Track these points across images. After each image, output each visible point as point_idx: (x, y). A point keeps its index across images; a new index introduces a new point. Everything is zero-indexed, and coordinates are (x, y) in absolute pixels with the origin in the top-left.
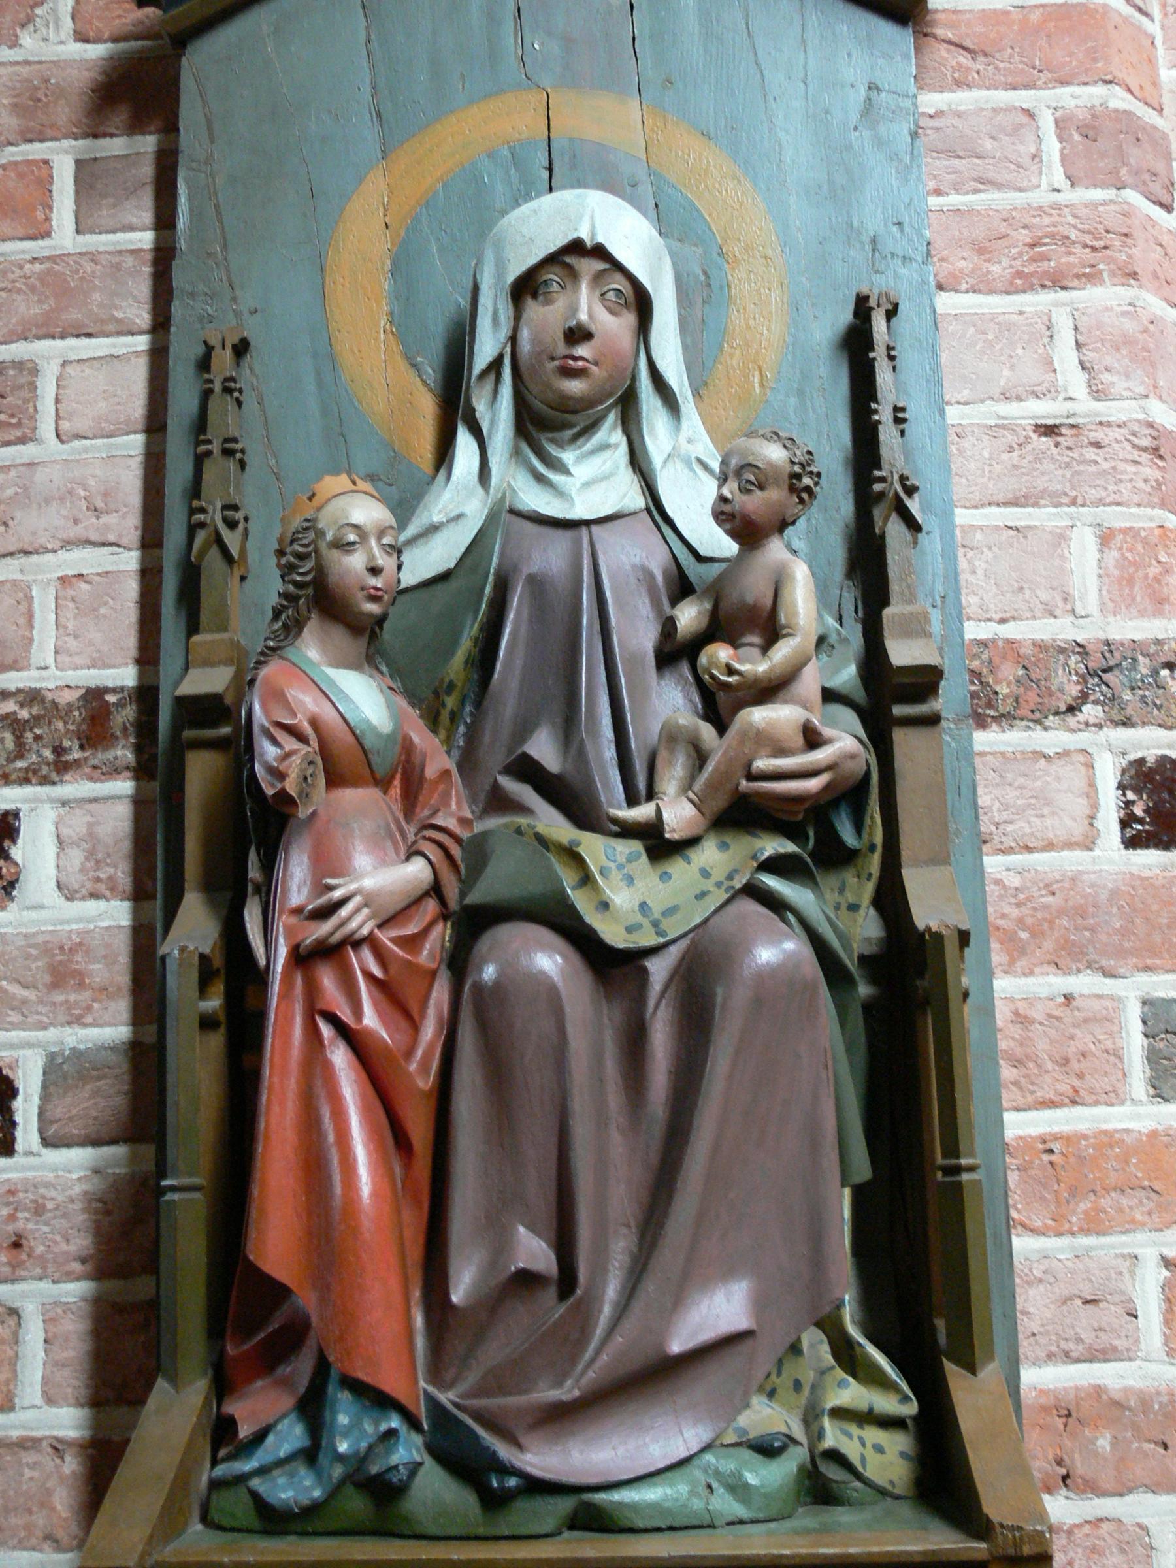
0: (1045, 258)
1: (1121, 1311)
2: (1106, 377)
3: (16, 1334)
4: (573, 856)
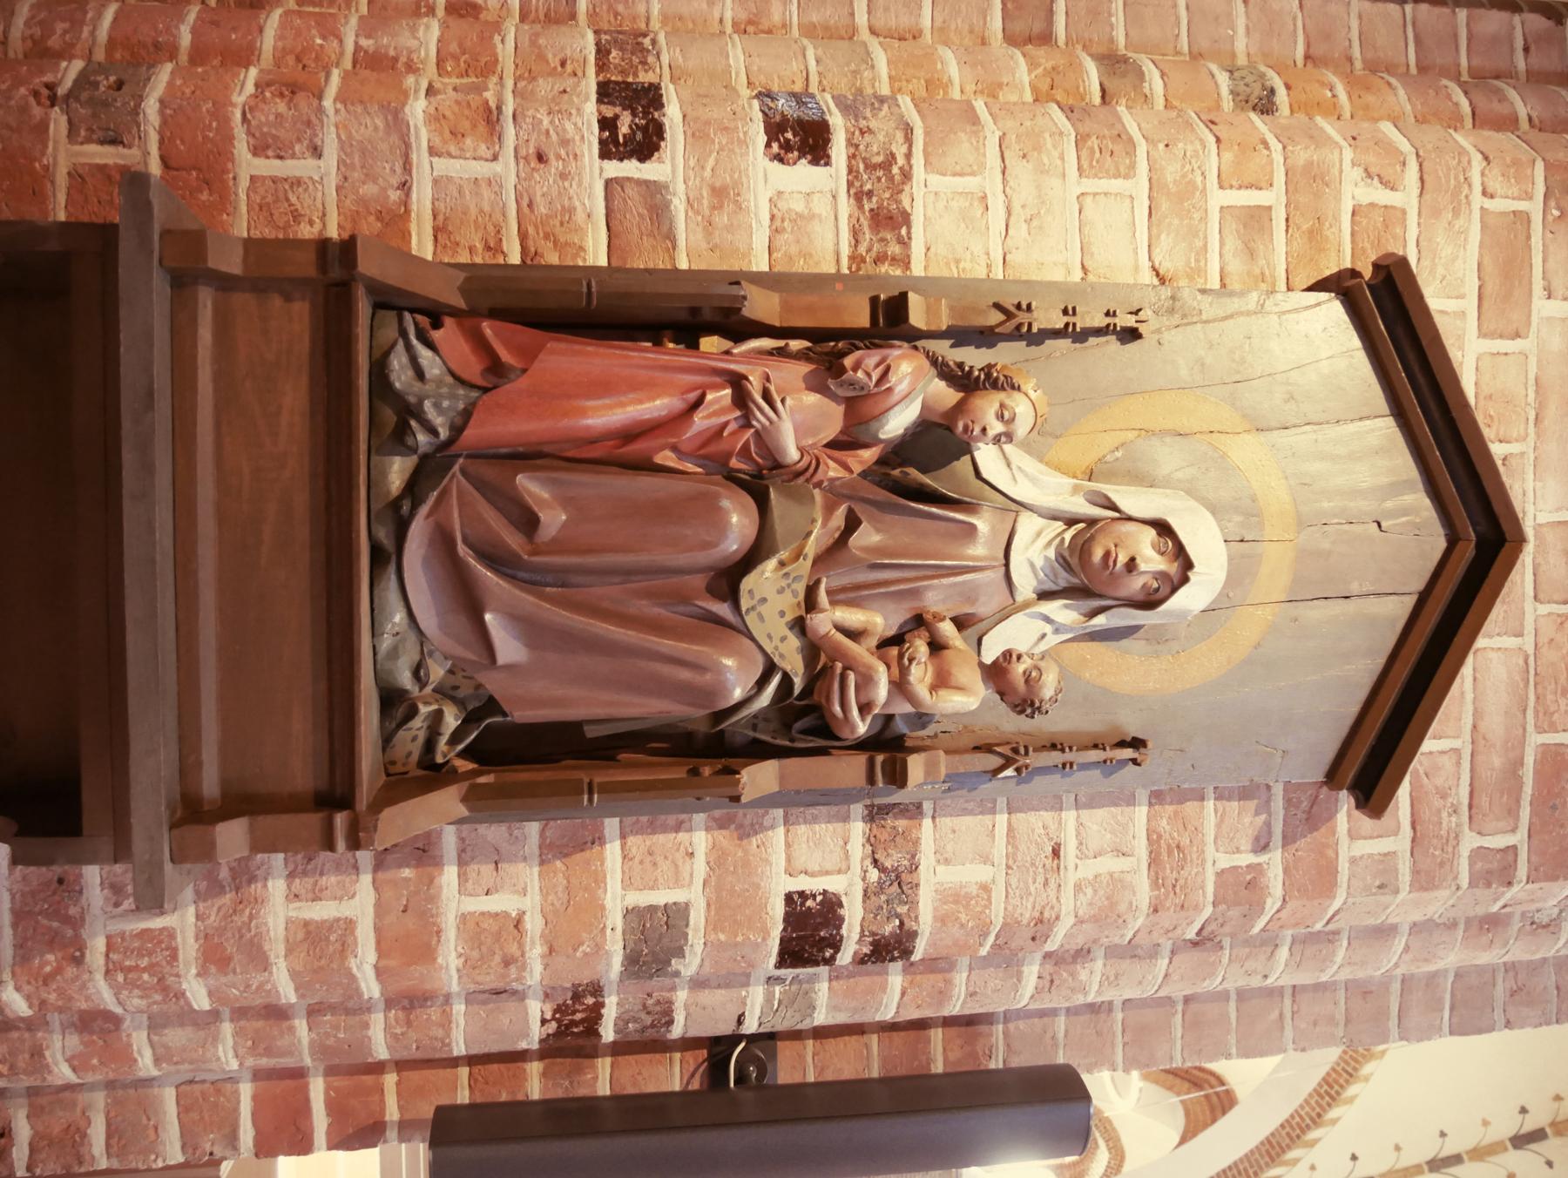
0: (1170, 853)
1: (491, 885)
2: (1089, 891)
3: (481, 158)
4: (798, 555)
